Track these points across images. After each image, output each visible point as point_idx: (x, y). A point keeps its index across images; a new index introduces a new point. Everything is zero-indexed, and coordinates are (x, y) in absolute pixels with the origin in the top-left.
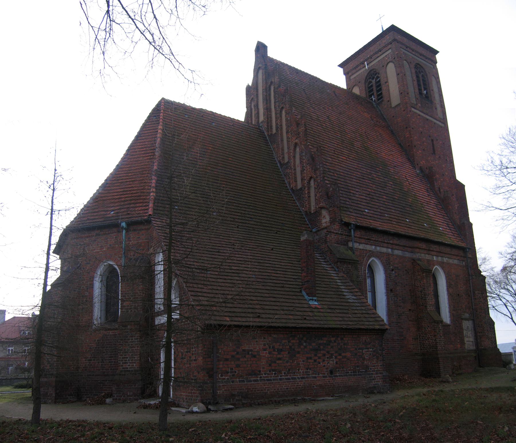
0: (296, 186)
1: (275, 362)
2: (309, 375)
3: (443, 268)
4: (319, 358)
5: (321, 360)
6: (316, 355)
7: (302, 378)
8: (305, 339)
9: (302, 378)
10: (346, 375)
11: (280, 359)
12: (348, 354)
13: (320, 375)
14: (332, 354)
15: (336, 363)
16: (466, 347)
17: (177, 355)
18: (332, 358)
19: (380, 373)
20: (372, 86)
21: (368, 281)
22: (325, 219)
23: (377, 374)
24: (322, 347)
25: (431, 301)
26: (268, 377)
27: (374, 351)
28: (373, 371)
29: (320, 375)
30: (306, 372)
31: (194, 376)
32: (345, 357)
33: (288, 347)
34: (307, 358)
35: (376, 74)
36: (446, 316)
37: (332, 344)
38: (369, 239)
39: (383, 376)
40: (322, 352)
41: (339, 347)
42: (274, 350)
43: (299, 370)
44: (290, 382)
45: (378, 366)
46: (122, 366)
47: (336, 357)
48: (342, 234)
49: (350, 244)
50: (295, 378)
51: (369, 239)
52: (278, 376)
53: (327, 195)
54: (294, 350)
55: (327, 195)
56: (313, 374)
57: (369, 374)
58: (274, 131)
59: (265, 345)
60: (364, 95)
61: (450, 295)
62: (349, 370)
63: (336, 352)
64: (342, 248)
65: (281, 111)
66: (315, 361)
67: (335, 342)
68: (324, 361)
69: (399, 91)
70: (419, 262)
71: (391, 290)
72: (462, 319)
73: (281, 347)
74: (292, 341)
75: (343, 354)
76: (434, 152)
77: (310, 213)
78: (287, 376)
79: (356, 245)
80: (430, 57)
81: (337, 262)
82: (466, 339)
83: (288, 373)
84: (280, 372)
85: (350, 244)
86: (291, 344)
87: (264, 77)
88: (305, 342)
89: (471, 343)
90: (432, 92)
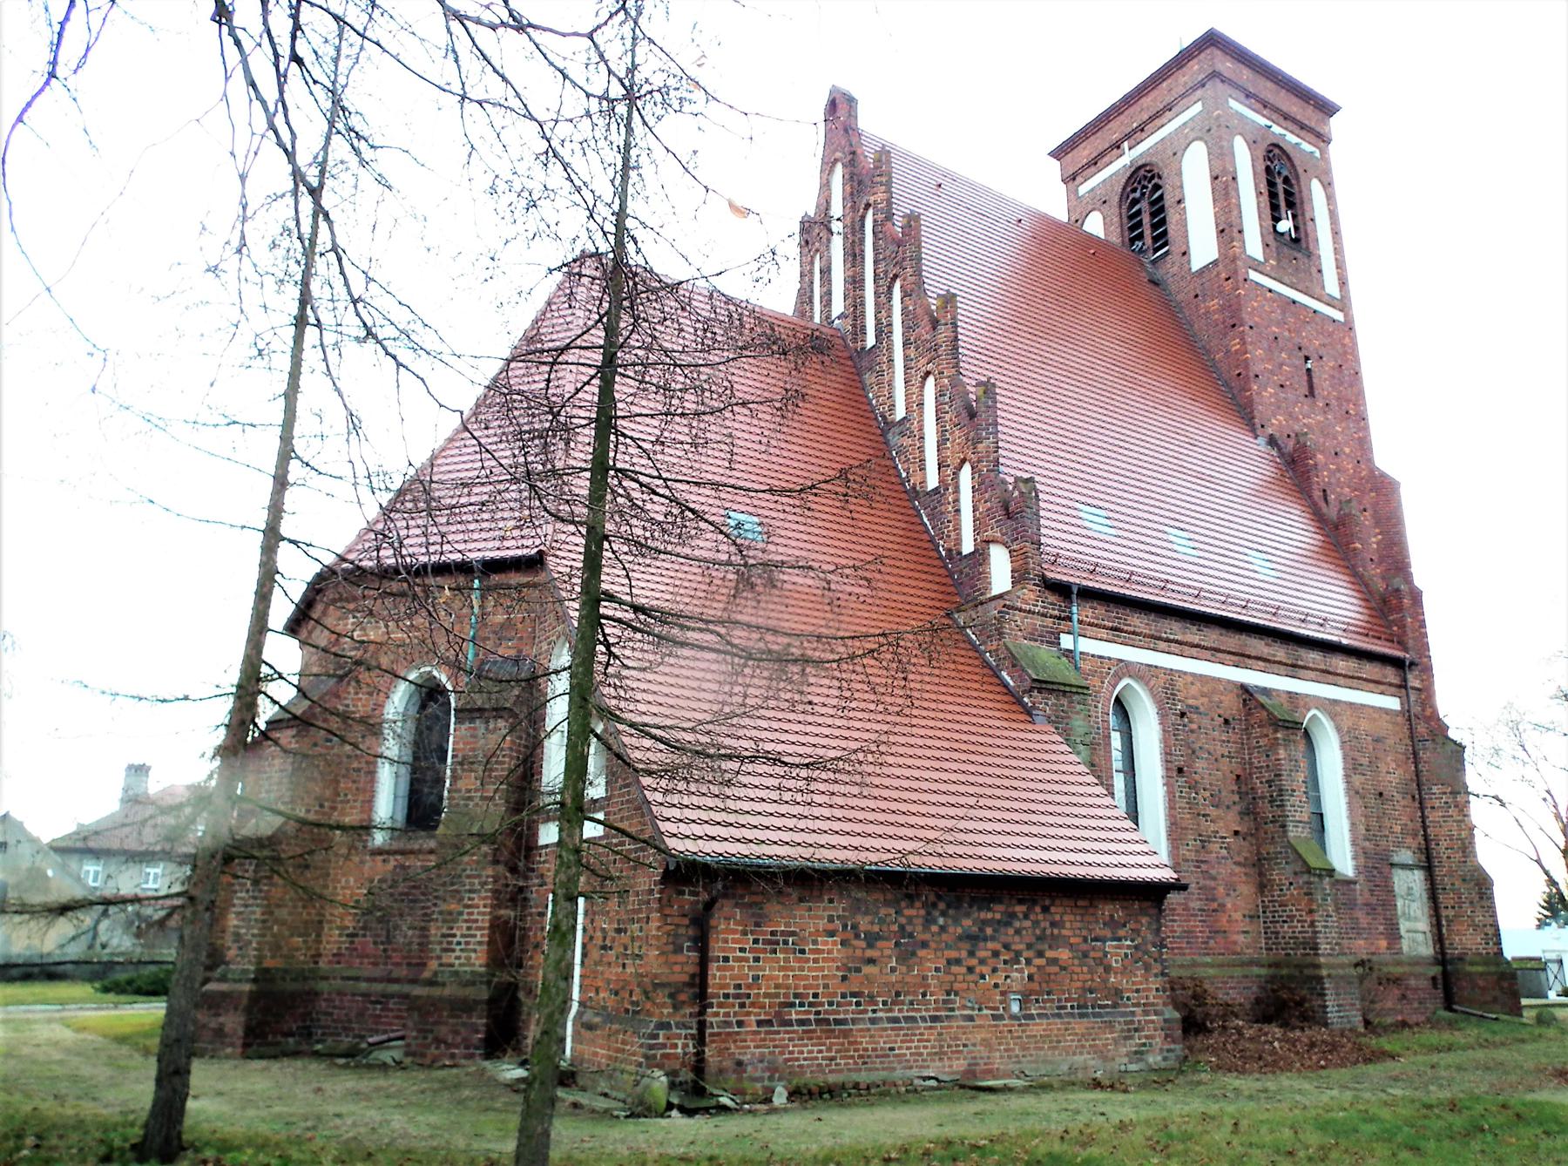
0: (923, 482)
1: (858, 970)
2: (952, 1010)
3: (1333, 717)
4: (982, 962)
5: (986, 970)
6: (972, 954)
7: (935, 1019)
8: (942, 906)
9: (935, 1019)
10: (1059, 1016)
11: (871, 961)
12: (1064, 954)
13: (985, 1012)
14: (1018, 954)
15: (1030, 978)
16: (1405, 948)
17: (591, 938)
18: (1018, 962)
19: (1156, 1013)
20: (1139, 212)
21: (1116, 740)
22: (1000, 572)
23: (1146, 1013)
24: (989, 931)
25: (1298, 811)
26: (838, 1013)
27: (1136, 947)
28: (1134, 1005)
29: (985, 1012)
30: (945, 1002)
31: (633, 1003)
32: (1054, 961)
33: (895, 928)
34: (949, 962)
35: (1153, 177)
36: (1342, 856)
37: (1017, 924)
38: (1116, 629)
39: (1165, 1021)
40: (990, 945)
41: (1038, 932)
42: (857, 936)
43: (924, 995)
44: (901, 1029)
45: (1149, 990)
46: (439, 958)
47: (1028, 962)
48: (1044, 615)
49: (1066, 641)
50: (913, 1019)
51: (1116, 629)
52: (865, 1011)
53: (1007, 509)
54: (911, 935)
55: (1007, 509)
56: (964, 1007)
57: (1124, 1014)
58: (871, 341)
59: (831, 919)
60: (1115, 239)
61: (1353, 792)
62: (1067, 1000)
63: (1029, 946)
64: (1044, 653)
65: (890, 288)
66: (970, 970)
67: (1026, 917)
68: (994, 970)
69: (1217, 225)
70: (1262, 699)
71: (1180, 770)
72: (1392, 865)
73: (876, 928)
74: (907, 912)
75: (1049, 954)
76: (1311, 392)
77: (960, 553)
78: (891, 1010)
79: (1087, 646)
80: (1313, 125)
81: (1032, 689)
82: (1404, 926)
83: (893, 1003)
84: (872, 1000)
85: (1066, 641)
86: (903, 920)
87: (848, 188)
88: (943, 914)
89: (1420, 937)
90: (1310, 223)
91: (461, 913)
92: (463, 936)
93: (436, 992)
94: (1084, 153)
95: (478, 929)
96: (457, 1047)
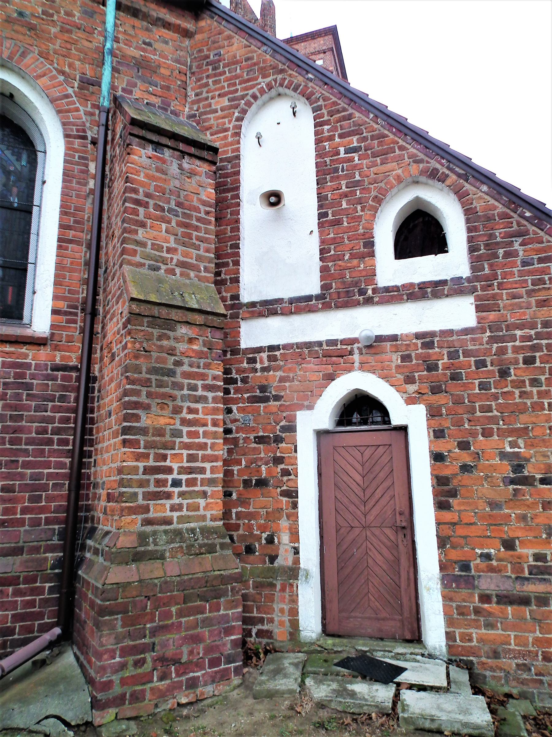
91: (177, 434)
92: (182, 470)
93: (152, 571)
94: (137, 131)
95: (205, 459)
96: (199, 666)
